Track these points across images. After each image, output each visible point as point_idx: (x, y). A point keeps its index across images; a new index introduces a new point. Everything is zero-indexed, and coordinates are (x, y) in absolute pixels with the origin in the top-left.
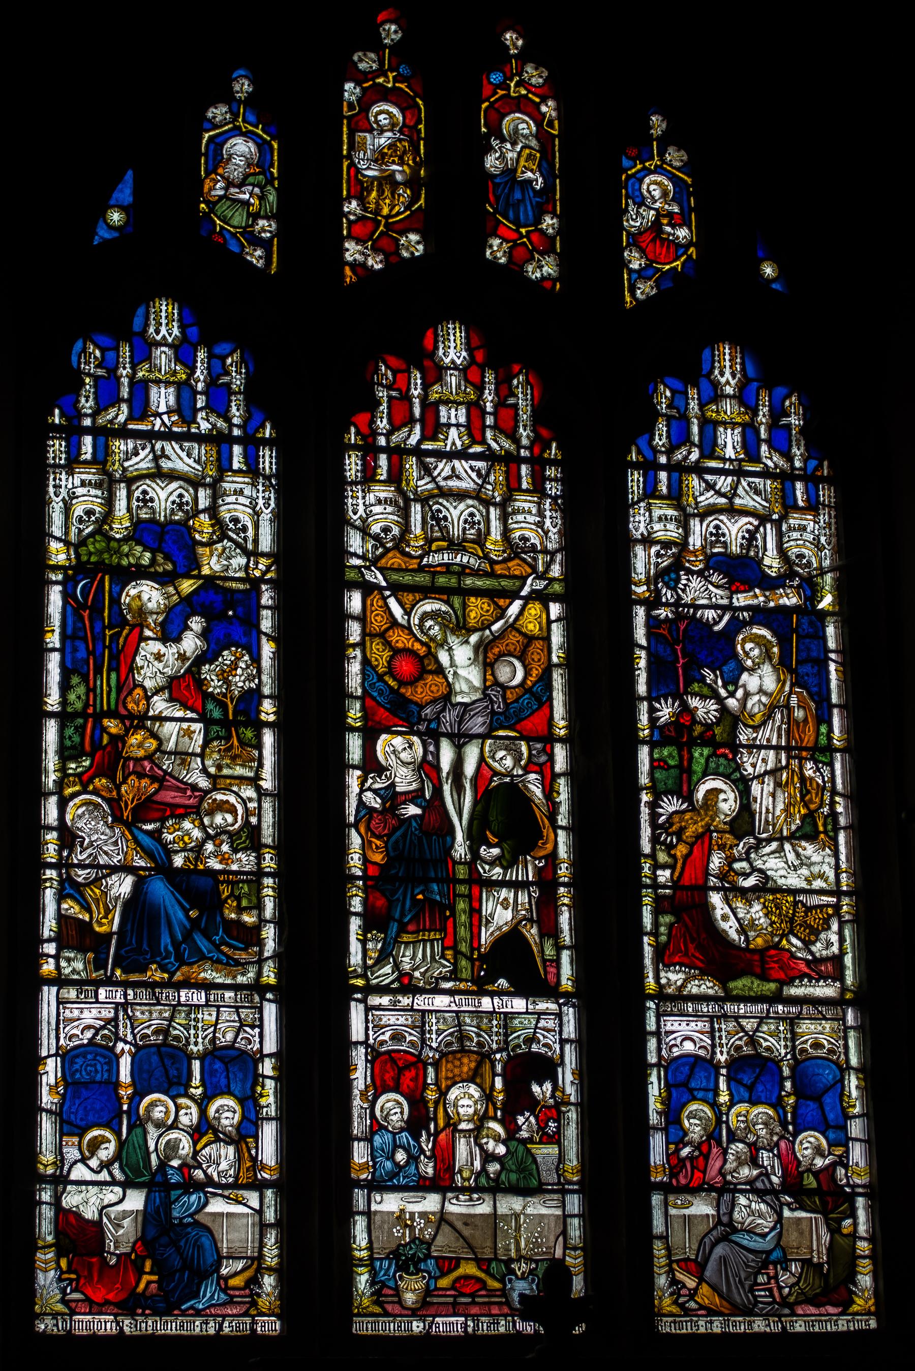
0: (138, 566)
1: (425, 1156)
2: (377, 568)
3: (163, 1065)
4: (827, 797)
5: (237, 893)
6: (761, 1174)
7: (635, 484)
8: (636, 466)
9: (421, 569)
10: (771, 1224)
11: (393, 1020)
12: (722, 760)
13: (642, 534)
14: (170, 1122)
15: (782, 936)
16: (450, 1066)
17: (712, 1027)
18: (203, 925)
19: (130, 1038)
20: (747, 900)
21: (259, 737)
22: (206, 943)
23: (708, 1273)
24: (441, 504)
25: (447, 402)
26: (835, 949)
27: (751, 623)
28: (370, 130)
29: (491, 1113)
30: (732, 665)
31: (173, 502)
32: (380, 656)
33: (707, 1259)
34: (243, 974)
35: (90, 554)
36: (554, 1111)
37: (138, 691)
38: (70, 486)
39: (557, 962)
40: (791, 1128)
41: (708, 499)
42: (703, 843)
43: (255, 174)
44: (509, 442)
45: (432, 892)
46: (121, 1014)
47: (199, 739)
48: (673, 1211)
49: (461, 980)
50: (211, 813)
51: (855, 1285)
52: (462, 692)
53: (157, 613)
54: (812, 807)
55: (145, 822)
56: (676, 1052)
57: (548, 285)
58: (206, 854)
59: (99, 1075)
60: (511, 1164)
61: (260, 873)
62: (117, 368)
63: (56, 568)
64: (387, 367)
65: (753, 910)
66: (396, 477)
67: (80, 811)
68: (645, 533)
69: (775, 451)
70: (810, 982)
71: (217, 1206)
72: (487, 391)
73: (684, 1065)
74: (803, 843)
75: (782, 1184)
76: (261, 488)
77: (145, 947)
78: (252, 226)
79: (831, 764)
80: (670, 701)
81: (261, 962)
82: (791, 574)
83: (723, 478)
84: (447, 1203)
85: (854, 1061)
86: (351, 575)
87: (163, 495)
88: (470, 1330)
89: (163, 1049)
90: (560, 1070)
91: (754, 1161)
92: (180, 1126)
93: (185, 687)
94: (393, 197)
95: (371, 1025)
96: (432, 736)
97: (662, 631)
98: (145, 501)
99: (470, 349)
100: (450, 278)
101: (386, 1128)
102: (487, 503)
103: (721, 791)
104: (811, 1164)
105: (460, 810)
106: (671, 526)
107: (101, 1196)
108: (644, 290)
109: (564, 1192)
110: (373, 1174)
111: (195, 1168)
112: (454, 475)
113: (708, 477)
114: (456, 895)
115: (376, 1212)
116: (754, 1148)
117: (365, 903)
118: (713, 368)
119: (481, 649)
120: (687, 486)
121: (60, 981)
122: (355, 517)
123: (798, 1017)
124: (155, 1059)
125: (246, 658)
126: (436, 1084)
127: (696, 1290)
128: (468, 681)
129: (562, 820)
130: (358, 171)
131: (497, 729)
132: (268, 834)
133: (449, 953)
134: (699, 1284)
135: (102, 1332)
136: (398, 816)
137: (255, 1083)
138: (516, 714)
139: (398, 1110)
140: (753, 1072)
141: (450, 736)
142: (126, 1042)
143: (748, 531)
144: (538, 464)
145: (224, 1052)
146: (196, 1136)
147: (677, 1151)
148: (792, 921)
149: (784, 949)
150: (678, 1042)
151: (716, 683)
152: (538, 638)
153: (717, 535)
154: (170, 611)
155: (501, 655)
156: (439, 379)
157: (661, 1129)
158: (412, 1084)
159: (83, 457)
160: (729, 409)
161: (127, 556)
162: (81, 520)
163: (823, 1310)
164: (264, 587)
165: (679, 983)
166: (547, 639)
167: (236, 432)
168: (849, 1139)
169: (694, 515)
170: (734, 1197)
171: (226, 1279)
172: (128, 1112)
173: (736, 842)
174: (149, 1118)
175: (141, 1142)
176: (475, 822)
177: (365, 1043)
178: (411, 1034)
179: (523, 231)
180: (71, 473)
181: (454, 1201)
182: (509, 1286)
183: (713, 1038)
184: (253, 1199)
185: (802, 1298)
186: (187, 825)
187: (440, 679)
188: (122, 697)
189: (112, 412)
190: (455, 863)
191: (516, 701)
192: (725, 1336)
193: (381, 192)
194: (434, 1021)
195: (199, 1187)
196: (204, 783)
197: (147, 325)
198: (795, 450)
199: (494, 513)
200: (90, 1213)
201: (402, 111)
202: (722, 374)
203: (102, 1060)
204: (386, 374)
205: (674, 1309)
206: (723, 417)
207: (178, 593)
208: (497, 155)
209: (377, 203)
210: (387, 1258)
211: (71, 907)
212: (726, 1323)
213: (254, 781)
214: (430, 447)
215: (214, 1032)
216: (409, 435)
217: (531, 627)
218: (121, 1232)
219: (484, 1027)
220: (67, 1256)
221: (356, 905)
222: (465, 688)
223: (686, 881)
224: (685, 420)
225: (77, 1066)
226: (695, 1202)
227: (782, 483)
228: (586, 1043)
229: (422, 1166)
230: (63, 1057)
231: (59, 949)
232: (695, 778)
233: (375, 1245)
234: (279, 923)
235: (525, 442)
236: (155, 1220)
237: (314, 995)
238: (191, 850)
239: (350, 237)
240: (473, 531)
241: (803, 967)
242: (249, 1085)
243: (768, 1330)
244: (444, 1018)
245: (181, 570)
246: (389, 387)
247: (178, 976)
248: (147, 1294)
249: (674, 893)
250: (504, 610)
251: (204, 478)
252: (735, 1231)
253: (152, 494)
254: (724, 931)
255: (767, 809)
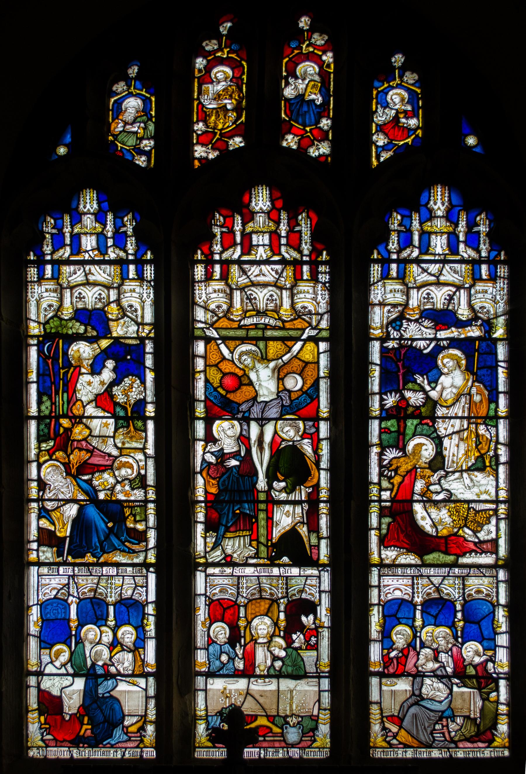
0: (77, 334)
1: (238, 658)
2: (214, 328)
3: (94, 610)
4: (492, 446)
5: (134, 513)
6: (440, 666)
7: (375, 272)
8: (376, 261)
9: (240, 327)
10: (446, 695)
11: (221, 582)
12: (425, 427)
13: (379, 301)
14: (97, 640)
15: (460, 528)
16: (253, 606)
17: (413, 583)
18: (115, 531)
19: (76, 594)
20: (437, 508)
21: (145, 425)
22: (117, 541)
23: (405, 724)
24: (252, 291)
25: (256, 232)
26: (493, 535)
27: (449, 347)
28: (212, 82)
29: (277, 633)
30: (434, 371)
31: (96, 298)
32: (215, 377)
33: (405, 716)
34: (137, 558)
35: (51, 328)
36: (314, 631)
37: (79, 403)
38: (40, 292)
39: (318, 546)
40: (460, 640)
41: (424, 278)
42: (411, 475)
43: (141, 116)
44: (296, 253)
45: (245, 509)
46: (71, 581)
47: (112, 428)
48: (384, 688)
49: (261, 558)
50: (119, 469)
51: (496, 730)
52: (264, 395)
53: (88, 359)
54: (483, 452)
55: (83, 475)
56: (390, 597)
57: (322, 159)
58: (117, 491)
59: (60, 615)
60: (288, 662)
61: (146, 501)
62: (63, 228)
63: (33, 337)
64: (220, 215)
65: (441, 513)
66: (225, 276)
67: (48, 470)
68: (381, 300)
69: (469, 247)
70: (476, 555)
71: (123, 687)
72: (282, 224)
73: (394, 604)
74: (476, 473)
75: (454, 672)
76: (145, 287)
77: (84, 543)
78: (139, 144)
79: (496, 426)
80: (393, 394)
81: (146, 551)
82: (476, 318)
83: (433, 265)
84: (251, 684)
85: (503, 600)
86: (198, 333)
87: (90, 294)
88: (262, 756)
89: (94, 600)
90: (318, 608)
91: (436, 659)
92: (103, 643)
93: (105, 400)
94: (225, 118)
95: (208, 585)
96: (246, 420)
97: (390, 355)
98: (80, 298)
99: (272, 201)
100: (260, 157)
101: (216, 642)
102: (281, 288)
103: (424, 444)
104: (472, 661)
105: (261, 461)
106: (398, 295)
107: (61, 682)
108: (385, 156)
109: (319, 677)
110: (209, 668)
111: (111, 666)
112: (261, 274)
113: (423, 265)
114: (259, 510)
115: (210, 689)
116: (436, 652)
117: (206, 516)
118: (429, 200)
119: (276, 370)
120: (409, 271)
121: (39, 564)
122: (200, 301)
123: (467, 576)
124: (89, 605)
125: (138, 381)
126: (245, 617)
127: (397, 733)
128: (267, 388)
129: (324, 464)
130: (203, 106)
131: (285, 415)
132: (151, 480)
133: (254, 543)
134: (399, 730)
135: (62, 757)
136: (225, 466)
137: (143, 618)
138: (298, 407)
139: (223, 632)
140: (438, 609)
141: (256, 420)
142: (74, 597)
143: (449, 295)
144: (314, 265)
145: (127, 601)
146: (112, 648)
147: (389, 653)
148: (466, 519)
149: (460, 536)
150: (391, 591)
151: (423, 382)
152: (312, 363)
153: (428, 298)
154: (96, 358)
155: (288, 373)
156: (252, 219)
157: (379, 641)
158: (231, 617)
159: (46, 277)
160: (440, 224)
161: (71, 328)
162: (46, 310)
163: (475, 745)
164: (147, 342)
165: (393, 557)
166: (318, 363)
167: (131, 257)
168: (496, 646)
169: (413, 288)
170: (423, 680)
171: (127, 728)
172: (75, 635)
173: (432, 474)
174: (86, 639)
175: (82, 652)
176: (271, 468)
177: (205, 595)
178: (231, 589)
179: (308, 129)
180: (40, 285)
181: (255, 683)
182: (285, 731)
183: (413, 589)
184: (142, 682)
185: (463, 738)
186: (106, 475)
187: (250, 388)
188: (70, 406)
189: (61, 252)
190: (258, 491)
191: (297, 399)
192: (414, 760)
193: (217, 116)
194: (245, 581)
195: (113, 676)
196: (115, 452)
197: (79, 204)
198: (482, 246)
199: (286, 294)
200: (55, 692)
201: (233, 69)
202: (435, 204)
203: (61, 607)
204: (219, 219)
205: (384, 744)
206: (435, 229)
207: (100, 348)
208: (293, 87)
209: (215, 123)
210: (216, 715)
211: (44, 523)
212: (415, 752)
213: (143, 450)
214: (246, 259)
215: (121, 590)
216: (234, 253)
217: (307, 356)
218: (72, 701)
219: (274, 584)
220: (44, 715)
221: (201, 517)
222: (266, 393)
223: (399, 498)
224: (409, 233)
225: (48, 610)
226: (398, 683)
227: (473, 266)
228: (334, 592)
229: (236, 664)
230: (41, 605)
231: (39, 546)
232: (407, 438)
233: (209, 708)
234: (158, 528)
235: (306, 252)
236: (89, 693)
237: (176, 568)
238: (108, 489)
239: (198, 143)
240: (272, 305)
241: (472, 546)
242: (140, 619)
243: (441, 756)
244: (251, 580)
245: (100, 335)
246: (221, 226)
247: (102, 560)
248: (86, 736)
249: (392, 505)
250: (290, 348)
251: (113, 284)
252: (423, 699)
253: (84, 294)
254: (422, 526)
255: (454, 455)
